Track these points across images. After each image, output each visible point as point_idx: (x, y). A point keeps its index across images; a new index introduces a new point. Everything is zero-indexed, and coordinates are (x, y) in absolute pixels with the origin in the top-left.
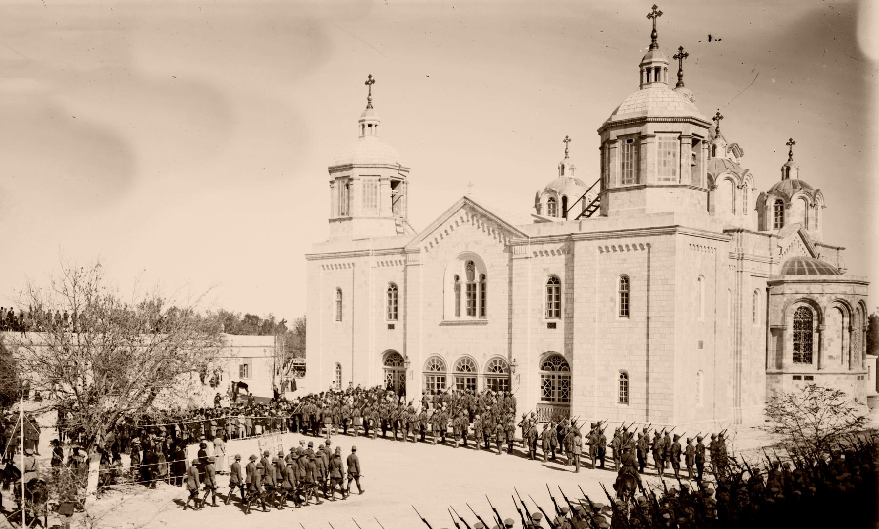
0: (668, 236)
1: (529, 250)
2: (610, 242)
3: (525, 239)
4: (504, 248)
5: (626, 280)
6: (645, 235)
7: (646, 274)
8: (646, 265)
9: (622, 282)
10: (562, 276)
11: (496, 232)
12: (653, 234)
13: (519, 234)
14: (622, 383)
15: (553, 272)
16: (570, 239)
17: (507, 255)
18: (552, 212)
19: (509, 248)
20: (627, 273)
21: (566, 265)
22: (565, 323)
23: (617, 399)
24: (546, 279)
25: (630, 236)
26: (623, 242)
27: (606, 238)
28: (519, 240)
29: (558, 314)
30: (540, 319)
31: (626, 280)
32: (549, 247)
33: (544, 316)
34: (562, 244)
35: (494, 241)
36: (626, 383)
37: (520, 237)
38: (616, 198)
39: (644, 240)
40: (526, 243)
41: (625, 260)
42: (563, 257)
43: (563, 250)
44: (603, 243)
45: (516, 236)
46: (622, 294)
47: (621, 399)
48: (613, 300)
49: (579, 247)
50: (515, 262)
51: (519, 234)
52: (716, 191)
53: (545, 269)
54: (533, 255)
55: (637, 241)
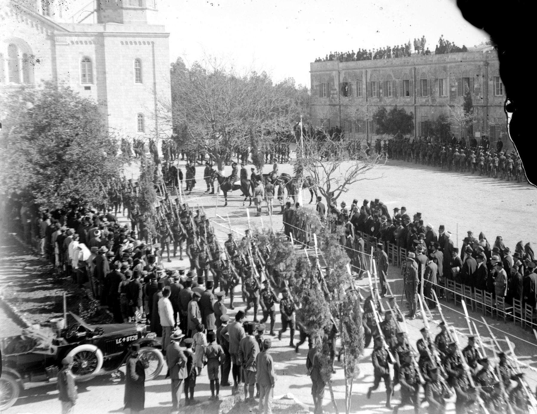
0: (164, 39)
1: (68, 39)
2: (129, 39)
3: (67, 33)
4: (45, 37)
5: (138, 61)
6: (150, 37)
7: (151, 58)
8: (151, 53)
9: (136, 62)
10: (93, 57)
11: (39, 26)
12: (156, 37)
13: (61, 29)
14: (139, 120)
15: (86, 54)
16: (101, 35)
17: (49, 42)
18: (498, 94)
19: (51, 38)
20: (140, 57)
21: (96, 51)
22: (246, 165)
23: (137, 129)
24: (80, 59)
25: (142, 36)
26: (137, 39)
27: (126, 36)
28: (62, 33)
29: (91, 81)
30: (78, 84)
31: (138, 61)
32: (84, 39)
33: (80, 82)
34: (93, 38)
35: (37, 32)
36: (142, 120)
37: (60, 31)
38: (128, 13)
39: (151, 40)
40: (66, 35)
41: (138, 50)
42: (93, 46)
43: (94, 41)
44: (124, 39)
45: (58, 30)
46: (136, 69)
47: (139, 130)
48: (131, 73)
49: (108, 41)
50: (57, 47)
51: (61, 29)
52: (467, 46)
53: (80, 53)
54: (70, 43)
55: (146, 40)
